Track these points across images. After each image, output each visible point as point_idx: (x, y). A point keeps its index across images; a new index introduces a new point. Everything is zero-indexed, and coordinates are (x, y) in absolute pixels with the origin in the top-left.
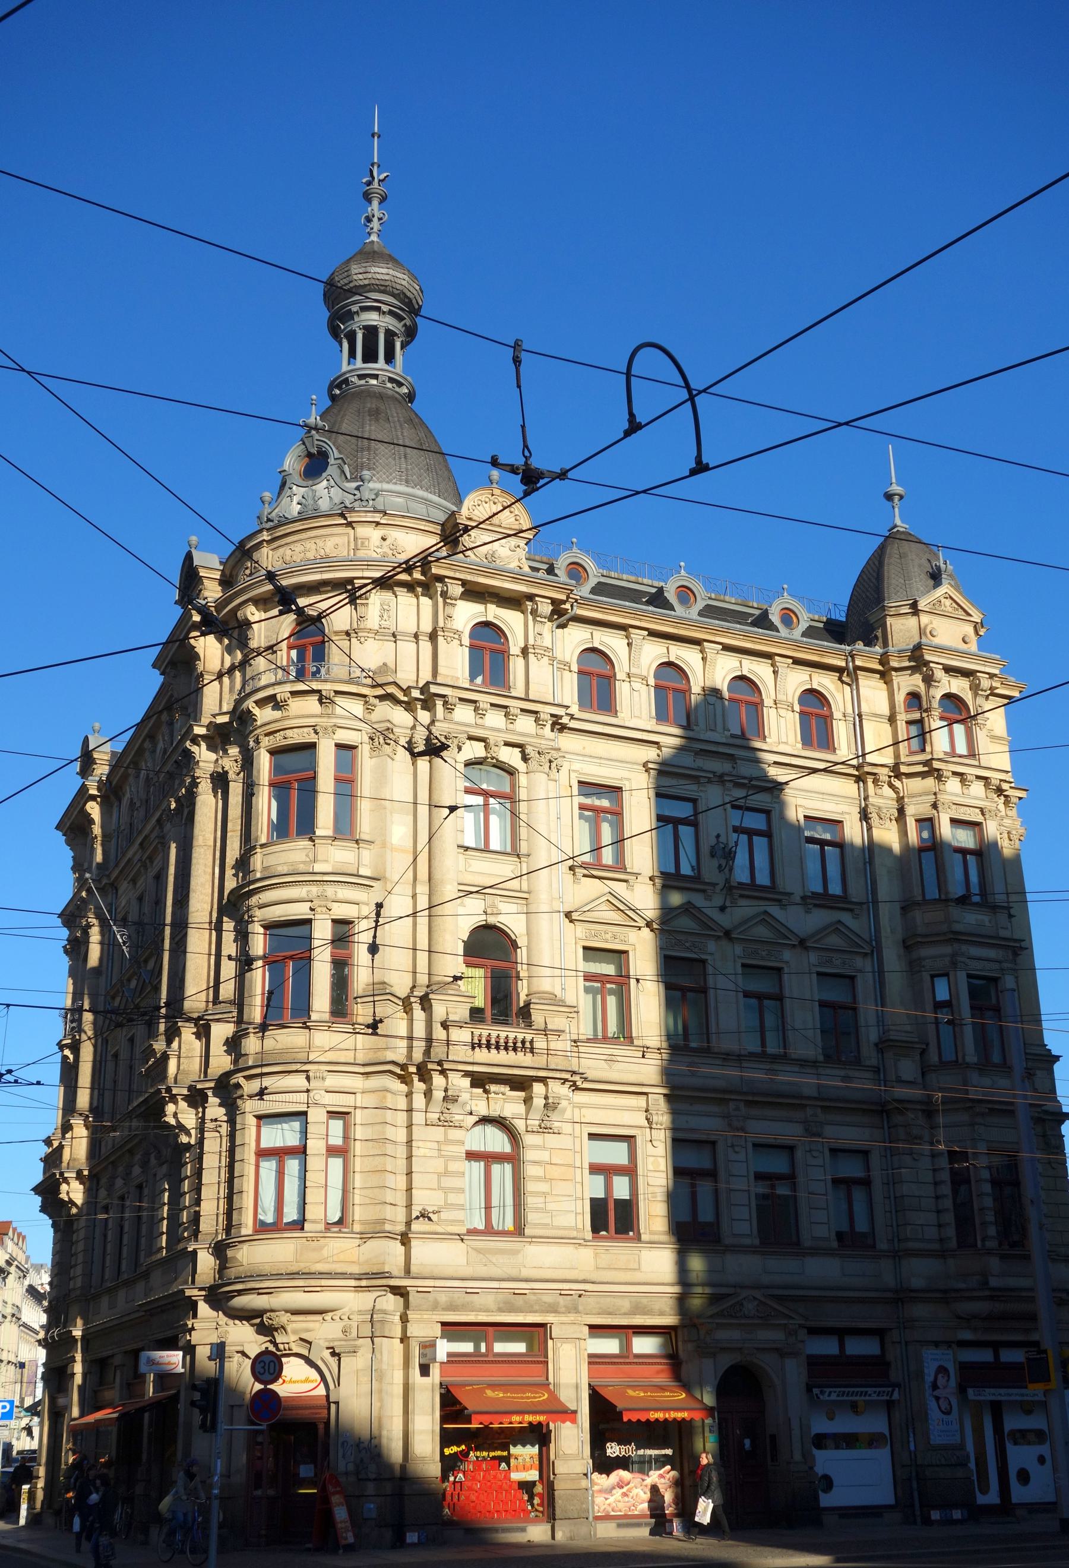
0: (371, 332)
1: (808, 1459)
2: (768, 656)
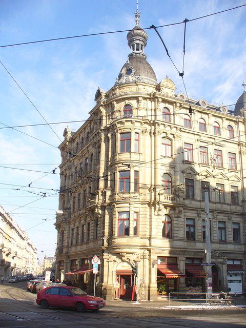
0: (138, 44)
1: (227, 285)
2: (221, 118)
